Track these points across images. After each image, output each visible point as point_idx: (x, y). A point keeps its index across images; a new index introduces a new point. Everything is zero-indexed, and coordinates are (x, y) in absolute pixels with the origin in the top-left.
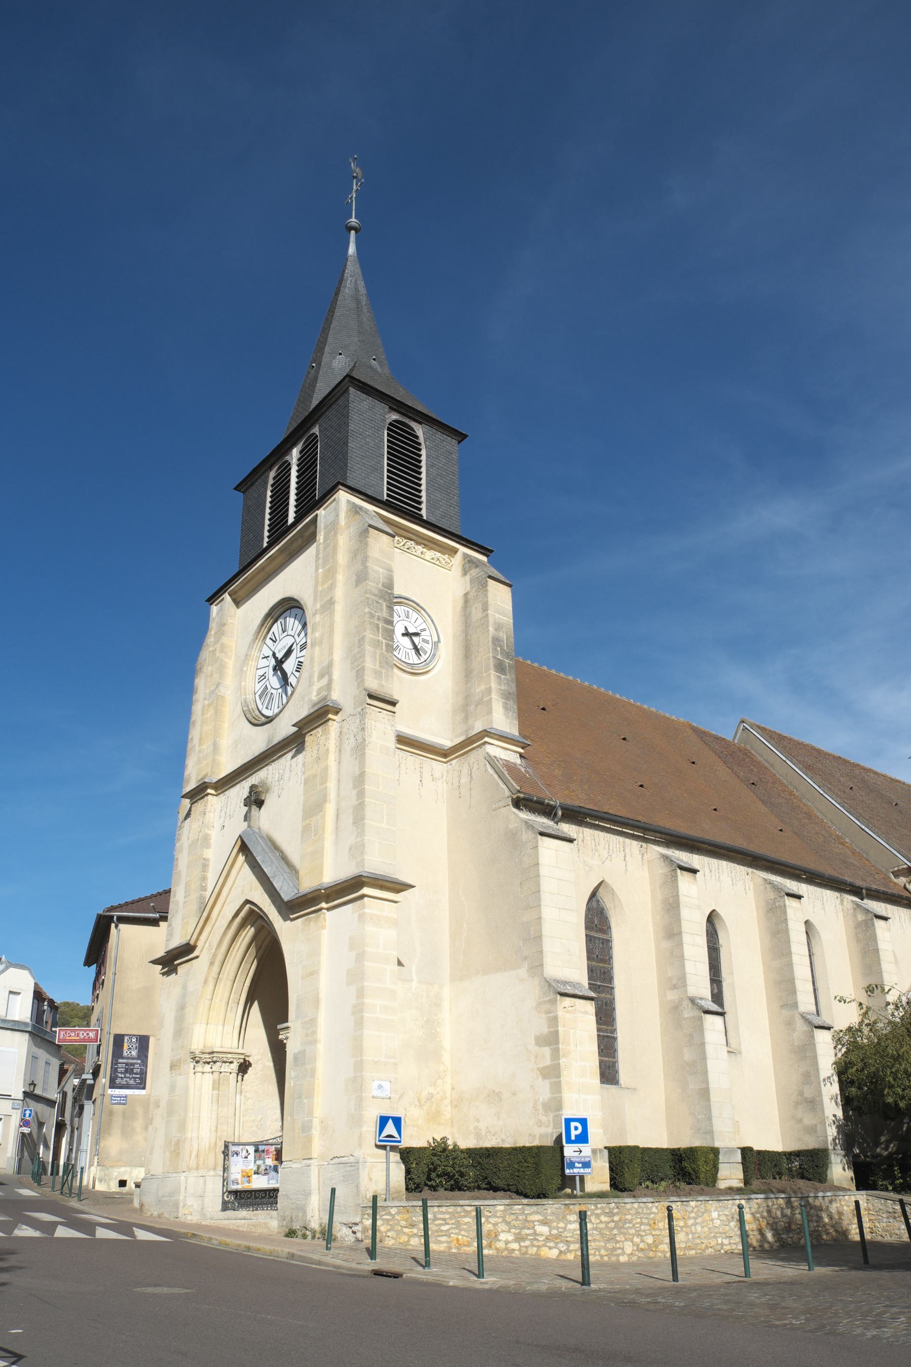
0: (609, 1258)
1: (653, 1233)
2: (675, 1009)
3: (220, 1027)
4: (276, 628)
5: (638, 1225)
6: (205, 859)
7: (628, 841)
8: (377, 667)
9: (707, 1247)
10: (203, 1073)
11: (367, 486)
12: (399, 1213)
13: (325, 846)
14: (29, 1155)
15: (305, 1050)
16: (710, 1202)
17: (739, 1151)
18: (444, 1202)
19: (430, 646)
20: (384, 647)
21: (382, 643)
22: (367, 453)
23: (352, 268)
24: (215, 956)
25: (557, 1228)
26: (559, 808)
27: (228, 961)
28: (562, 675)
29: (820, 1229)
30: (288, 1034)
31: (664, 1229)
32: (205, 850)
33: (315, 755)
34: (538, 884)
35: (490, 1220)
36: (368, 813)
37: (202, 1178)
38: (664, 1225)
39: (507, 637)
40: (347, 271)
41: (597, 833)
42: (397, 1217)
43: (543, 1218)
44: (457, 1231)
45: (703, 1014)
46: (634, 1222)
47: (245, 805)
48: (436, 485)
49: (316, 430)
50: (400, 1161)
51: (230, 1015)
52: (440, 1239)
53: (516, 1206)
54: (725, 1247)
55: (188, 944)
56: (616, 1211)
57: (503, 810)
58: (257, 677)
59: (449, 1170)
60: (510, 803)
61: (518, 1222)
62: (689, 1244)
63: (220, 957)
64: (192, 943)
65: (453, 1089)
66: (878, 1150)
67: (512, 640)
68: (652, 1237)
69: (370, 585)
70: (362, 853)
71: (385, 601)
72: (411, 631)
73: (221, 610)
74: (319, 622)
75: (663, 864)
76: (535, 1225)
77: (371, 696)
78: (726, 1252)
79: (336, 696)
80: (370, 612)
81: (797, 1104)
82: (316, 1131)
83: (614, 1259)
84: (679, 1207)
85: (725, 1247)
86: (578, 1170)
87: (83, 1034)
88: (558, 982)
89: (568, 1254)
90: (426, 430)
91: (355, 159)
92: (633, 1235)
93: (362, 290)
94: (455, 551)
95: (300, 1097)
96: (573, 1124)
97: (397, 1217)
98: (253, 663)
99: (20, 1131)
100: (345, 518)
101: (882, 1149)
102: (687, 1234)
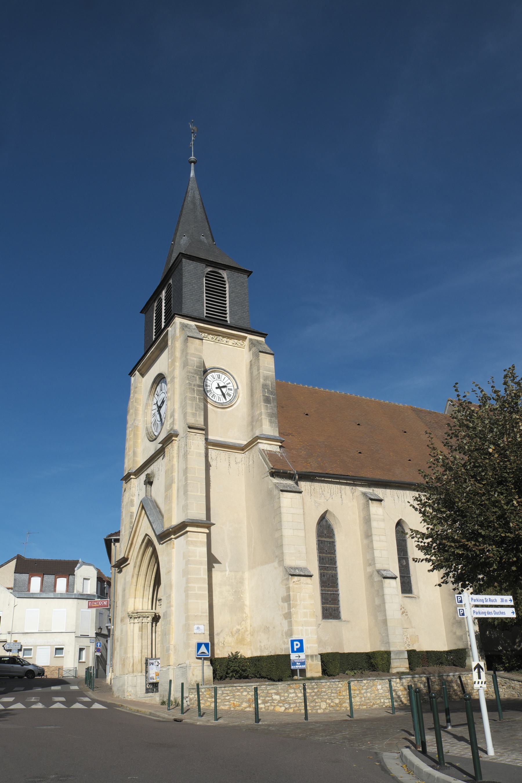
0: (312, 711)
1: (339, 697)
2: (370, 577)
3: (141, 599)
4: (158, 389)
5: (330, 694)
6: (131, 512)
7: (343, 487)
8: (194, 411)
9: (374, 704)
10: (134, 623)
11: (194, 311)
12: (205, 691)
13: (173, 506)
14: (102, 667)
15: (167, 611)
16: (376, 680)
17: (406, 652)
18: (227, 685)
19: (233, 392)
20: (198, 400)
21: (197, 398)
22: (194, 293)
23: (193, 185)
24: (136, 563)
25: (284, 696)
26: (297, 475)
27: (142, 566)
28: (327, 390)
29: (451, 693)
30: (161, 603)
31: (346, 695)
32: (132, 508)
33: (168, 458)
34: (281, 518)
35: (250, 693)
36: (190, 489)
37: (135, 677)
38: (346, 693)
39: (271, 383)
40: (189, 187)
41: (322, 485)
42: (205, 693)
43: (276, 691)
44: (233, 699)
45: (383, 579)
46: (327, 692)
47: (144, 485)
48: (235, 303)
49: (171, 281)
50: (210, 665)
51: (146, 593)
52: (225, 703)
53: (262, 686)
54: (385, 704)
55: (124, 557)
56: (315, 686)
57: (266, 478)
58: (152, 415)
59: (236, 669)
60: (269, 475)
61: (264, 694)
62: (362, 703)
63: (138, 563)
64: (126, 556)
65: (251, 626)
66: (515, 647)
67: (275, 384)
68: (338, 700)
69: (189, 368)
70: (187, 509)
71: (198, 375)
72: (221, 385)
73: (135, 380)
74: (170, 388)
75: (363, 498)
76: (272, 695)
77: (190, 427)
78: (386, 707)
79: (176, 427)
80: (189, 383)
81: (453, 624)
82: (172, 651)
83: (314, 711)
84: (356, 684)
85: (385, 704)
86: (298, 666)
87: (101, 603)
88: (292, 568)
89: (290, 709)
90: (228, 273)
91: (193, 122)
92: (327, 699)
93: (198, 197)
94: (245, 338)
95: (165, 635)
96: (295, 643)
97: (205, 693)
98: (150, 407)
99: (95, 654)
100: (179, 332)
101: (518, 646)
102: (361, 698)
